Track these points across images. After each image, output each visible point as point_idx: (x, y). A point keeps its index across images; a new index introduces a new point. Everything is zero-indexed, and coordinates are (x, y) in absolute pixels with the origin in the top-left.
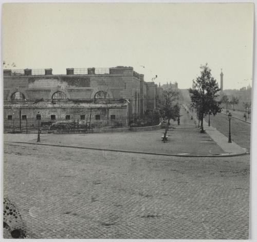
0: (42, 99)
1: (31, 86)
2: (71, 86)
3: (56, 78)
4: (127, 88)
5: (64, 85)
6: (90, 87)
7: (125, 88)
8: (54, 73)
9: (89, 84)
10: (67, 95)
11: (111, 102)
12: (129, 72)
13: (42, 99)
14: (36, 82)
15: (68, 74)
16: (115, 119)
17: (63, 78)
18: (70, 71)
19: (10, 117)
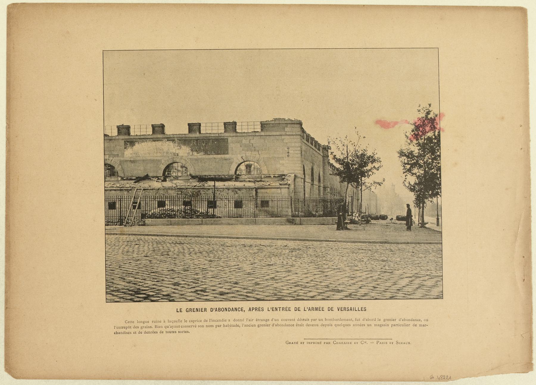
0: (147, 175)
1: (129, 153)
2: (195, 153)
3: (170, 139)
4: (291, 155)
5: (184, 151)
6: (227, 154)
7: (288, 156)
8: (168, 131)
9: (227, 150)
10: (392, 248)
11: (263, 180)
12: (209, 145)
13: (147, 175)
14: (137, 146)
15: (190, 131)
16: (268, 206)
17: (183, 141)
18: (193, 127)
19: (6, 270)
